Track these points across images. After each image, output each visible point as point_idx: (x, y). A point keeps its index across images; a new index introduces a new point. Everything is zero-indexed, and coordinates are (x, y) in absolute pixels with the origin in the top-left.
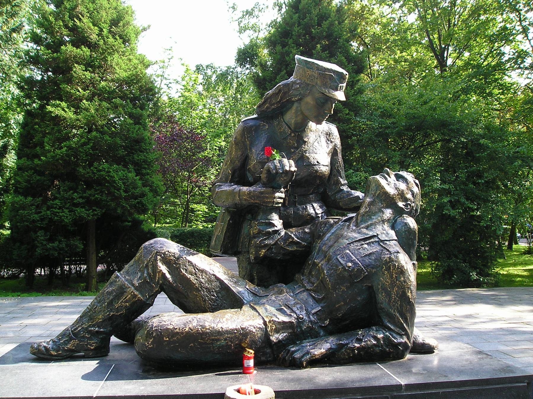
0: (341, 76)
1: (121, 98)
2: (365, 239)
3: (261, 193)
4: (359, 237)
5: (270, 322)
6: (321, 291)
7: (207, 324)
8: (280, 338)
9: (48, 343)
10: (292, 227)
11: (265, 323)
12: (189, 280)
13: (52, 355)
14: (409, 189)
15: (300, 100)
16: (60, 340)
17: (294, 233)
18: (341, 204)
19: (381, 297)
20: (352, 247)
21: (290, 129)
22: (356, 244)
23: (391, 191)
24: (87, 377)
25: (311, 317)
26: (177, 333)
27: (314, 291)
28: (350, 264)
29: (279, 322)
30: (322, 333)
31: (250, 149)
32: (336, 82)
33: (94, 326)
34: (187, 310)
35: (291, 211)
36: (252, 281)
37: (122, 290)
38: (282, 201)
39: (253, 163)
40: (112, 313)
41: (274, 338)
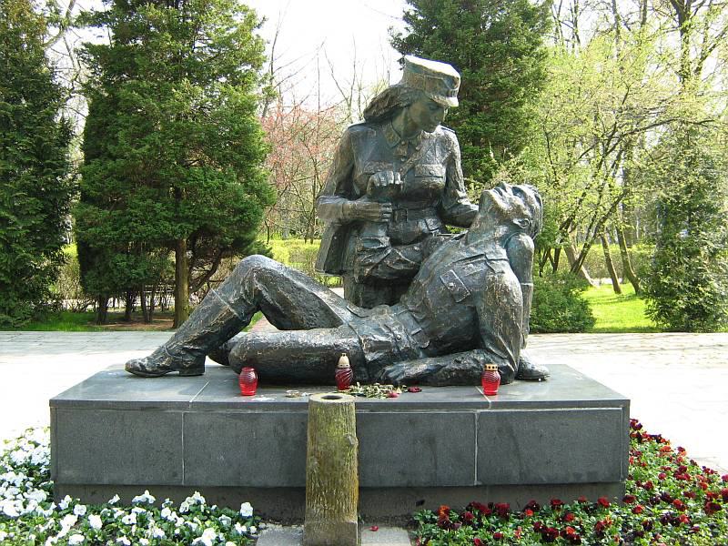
0: (452, 80)
2: (470, 258)
3: (367, 207)
4: (466, 255)
5: (365, 340)
6: (424, 313)
7: (300, 340)
8: (376, 357)
9: (143, 360)
10: (401, 244)
11: (360, 342)
12: (285, 298)
14: (527, 203)
15: (409, 106)
16: (155, 357)
17: (401, 253)
18: (457, 220)
19: (484, 318)
20: (457, 266)
23: (504, 205)
24: (180, 393)
25: (410, 337)
26: (271, 348)
27: (417, 312)
28: (452, 284)
29: (375, 342)
30: (421, 354)
31: (357, 158)
32: (446, 87)
34: (281, 327)
35: (401, 226)
36: (356, 303)
37: (218, 307)
38: (388, 215)
39: (359, 174)
41: (369, 357)
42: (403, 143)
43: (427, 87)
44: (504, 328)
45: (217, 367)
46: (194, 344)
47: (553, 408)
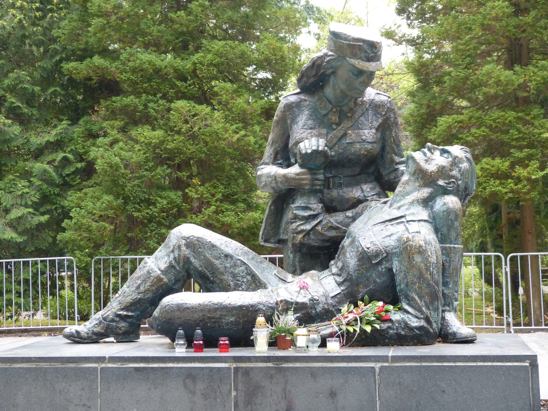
42: (334, 110)
43: (348, 53)
44: (420, 288)
45: (162, 345)
46: (127, 311)
47: (455, 362)
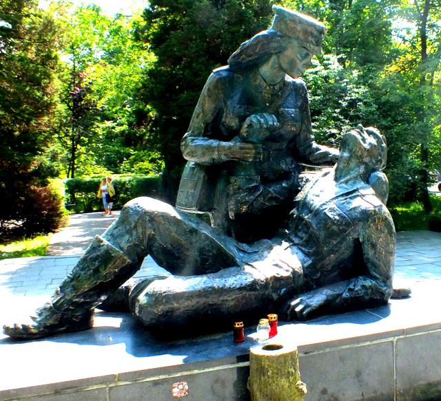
1: (9, 82)
13: (32, 334)
21: (265, 82)
22: (340, 198)
27: (302, 245)
33: (78, 297)
40: (99, 281)
